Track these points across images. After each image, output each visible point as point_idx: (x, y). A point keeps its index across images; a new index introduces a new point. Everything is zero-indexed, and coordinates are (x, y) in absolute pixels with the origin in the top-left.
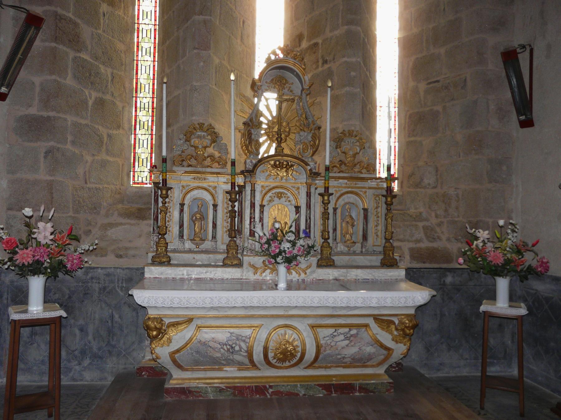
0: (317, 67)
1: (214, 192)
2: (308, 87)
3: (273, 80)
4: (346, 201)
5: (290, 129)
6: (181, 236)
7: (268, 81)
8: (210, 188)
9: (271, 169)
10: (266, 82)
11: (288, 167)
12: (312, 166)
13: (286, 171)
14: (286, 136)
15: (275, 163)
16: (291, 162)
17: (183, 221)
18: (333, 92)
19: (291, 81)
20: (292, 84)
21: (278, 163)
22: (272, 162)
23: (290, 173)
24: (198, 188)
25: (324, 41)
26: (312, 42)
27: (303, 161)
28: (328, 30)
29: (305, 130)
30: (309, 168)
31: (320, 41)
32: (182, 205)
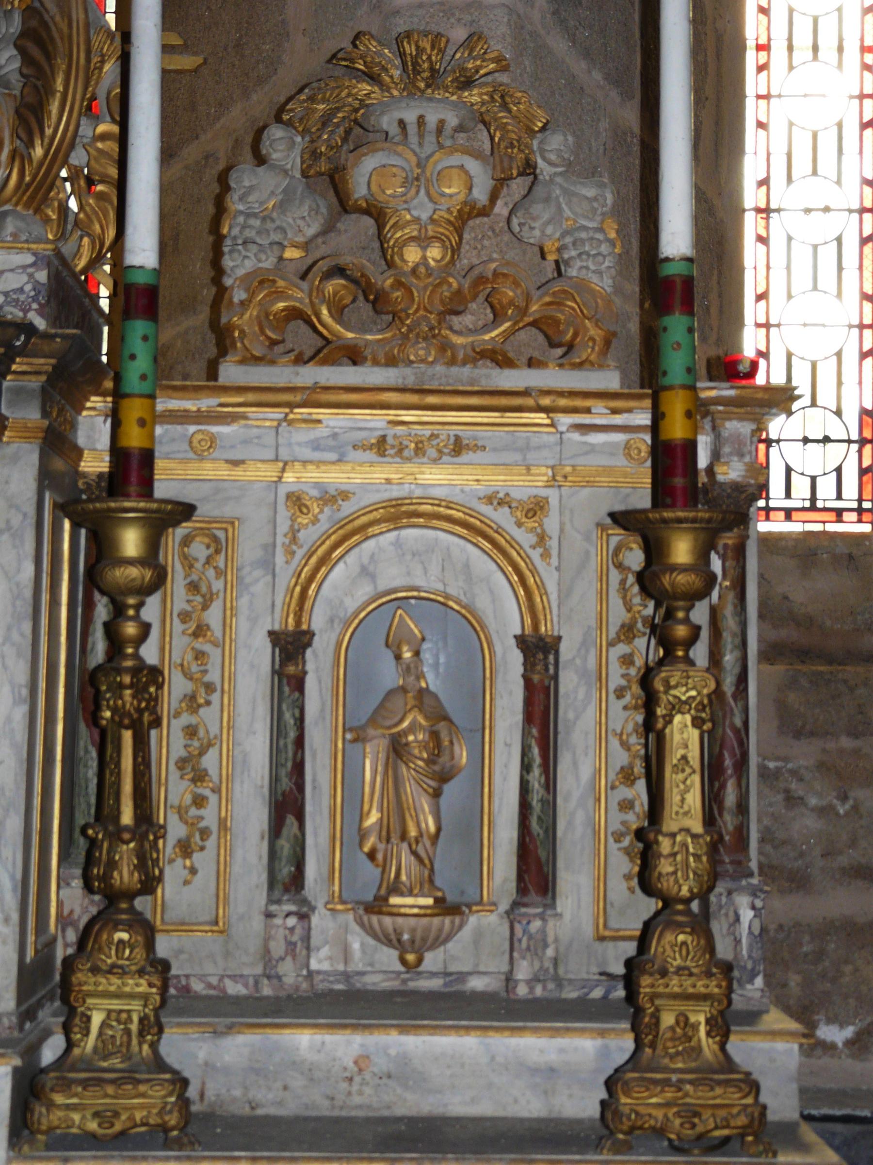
1: (525, 538)
4: (392, 576)
6: (287, 879)
8: (502, 517)
17: (299, 768)
24: (399, 513)
32: (291, 646)
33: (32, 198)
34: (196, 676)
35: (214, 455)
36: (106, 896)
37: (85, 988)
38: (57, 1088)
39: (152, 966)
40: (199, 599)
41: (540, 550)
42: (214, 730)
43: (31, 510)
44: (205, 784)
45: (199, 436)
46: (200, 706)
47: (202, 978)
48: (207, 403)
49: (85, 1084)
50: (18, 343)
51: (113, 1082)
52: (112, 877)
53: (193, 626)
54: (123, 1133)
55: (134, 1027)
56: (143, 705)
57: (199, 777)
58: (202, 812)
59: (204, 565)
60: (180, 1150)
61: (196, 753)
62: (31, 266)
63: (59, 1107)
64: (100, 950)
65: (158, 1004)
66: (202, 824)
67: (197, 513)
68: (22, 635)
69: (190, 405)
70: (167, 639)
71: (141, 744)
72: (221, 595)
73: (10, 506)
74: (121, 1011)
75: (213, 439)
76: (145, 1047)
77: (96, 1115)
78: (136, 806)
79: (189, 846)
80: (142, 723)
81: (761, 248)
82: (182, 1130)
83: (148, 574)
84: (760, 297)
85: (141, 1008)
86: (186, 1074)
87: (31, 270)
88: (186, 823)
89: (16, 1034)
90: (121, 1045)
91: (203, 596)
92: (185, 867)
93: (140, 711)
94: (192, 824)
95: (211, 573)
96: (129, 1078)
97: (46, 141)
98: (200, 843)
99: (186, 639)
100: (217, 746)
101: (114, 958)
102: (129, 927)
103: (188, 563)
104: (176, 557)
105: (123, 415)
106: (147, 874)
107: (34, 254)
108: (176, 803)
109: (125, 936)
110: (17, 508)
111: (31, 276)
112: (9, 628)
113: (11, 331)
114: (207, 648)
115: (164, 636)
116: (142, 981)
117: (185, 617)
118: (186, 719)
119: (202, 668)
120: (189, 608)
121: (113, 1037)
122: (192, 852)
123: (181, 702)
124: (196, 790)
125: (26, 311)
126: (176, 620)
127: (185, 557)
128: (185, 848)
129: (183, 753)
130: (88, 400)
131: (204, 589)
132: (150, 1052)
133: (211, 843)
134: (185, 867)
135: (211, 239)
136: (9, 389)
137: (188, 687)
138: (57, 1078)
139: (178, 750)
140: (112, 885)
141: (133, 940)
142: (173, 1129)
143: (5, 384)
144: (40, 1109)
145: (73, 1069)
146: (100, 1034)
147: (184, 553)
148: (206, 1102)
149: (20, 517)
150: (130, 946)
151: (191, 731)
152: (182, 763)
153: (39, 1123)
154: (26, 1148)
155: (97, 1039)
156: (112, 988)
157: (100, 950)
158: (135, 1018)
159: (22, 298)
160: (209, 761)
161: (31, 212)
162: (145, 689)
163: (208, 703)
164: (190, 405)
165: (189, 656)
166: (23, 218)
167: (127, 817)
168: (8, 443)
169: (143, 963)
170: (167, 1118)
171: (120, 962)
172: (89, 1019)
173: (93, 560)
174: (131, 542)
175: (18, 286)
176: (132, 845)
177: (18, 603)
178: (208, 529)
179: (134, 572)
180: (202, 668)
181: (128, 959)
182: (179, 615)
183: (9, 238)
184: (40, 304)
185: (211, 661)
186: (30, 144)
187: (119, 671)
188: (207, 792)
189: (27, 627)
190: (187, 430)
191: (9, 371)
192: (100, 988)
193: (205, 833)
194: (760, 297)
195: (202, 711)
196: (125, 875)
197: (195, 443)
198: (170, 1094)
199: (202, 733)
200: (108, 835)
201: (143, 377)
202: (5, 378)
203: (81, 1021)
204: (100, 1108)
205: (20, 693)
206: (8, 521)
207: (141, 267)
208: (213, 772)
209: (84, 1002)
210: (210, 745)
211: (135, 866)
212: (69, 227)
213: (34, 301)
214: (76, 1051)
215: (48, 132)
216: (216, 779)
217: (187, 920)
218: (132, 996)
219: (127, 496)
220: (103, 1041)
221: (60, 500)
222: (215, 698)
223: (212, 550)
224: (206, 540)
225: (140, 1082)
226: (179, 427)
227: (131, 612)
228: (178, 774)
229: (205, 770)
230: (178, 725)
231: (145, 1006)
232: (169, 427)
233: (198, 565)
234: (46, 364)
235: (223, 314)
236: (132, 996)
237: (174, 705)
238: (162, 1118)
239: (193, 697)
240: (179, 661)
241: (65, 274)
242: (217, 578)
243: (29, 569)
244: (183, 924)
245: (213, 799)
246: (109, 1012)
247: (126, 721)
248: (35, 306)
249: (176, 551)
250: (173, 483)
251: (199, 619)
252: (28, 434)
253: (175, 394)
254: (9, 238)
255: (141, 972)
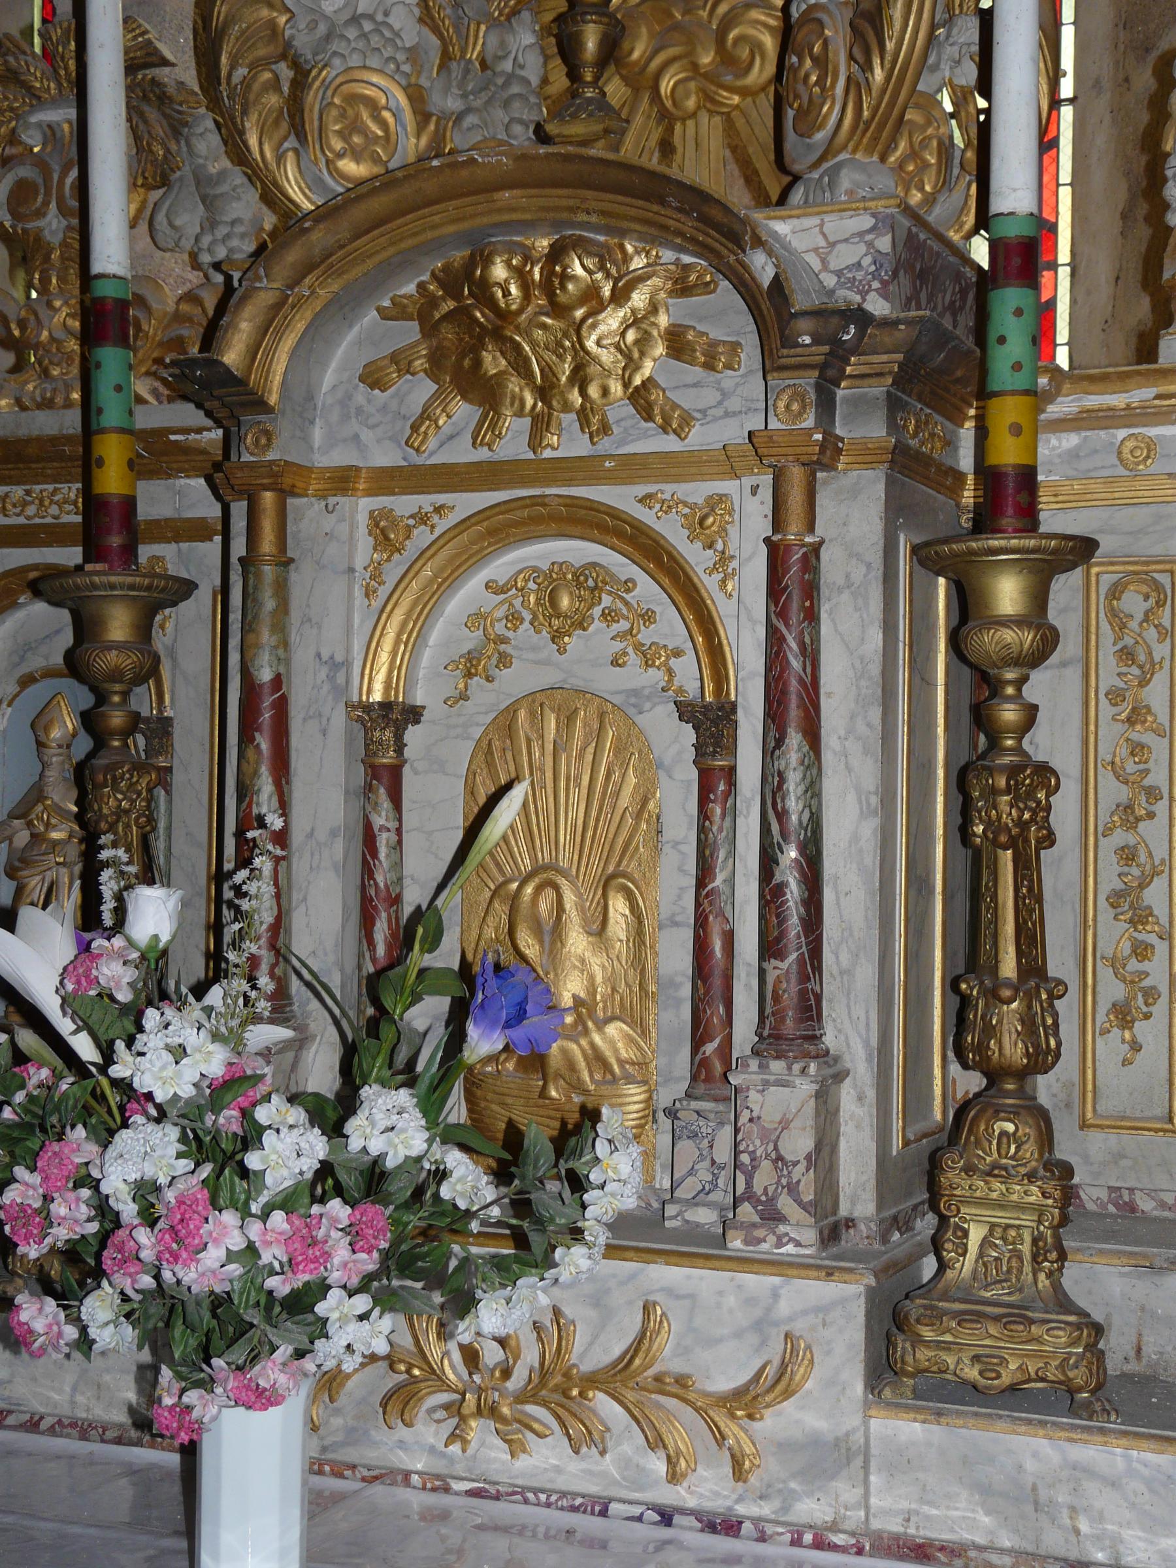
33: (875, 139)
34: (1132, 778)
35: (1152, 470)
36: (985, 1074)
37: (958, 1192)
38: (926, 1321)
39: (1045, 1168)
40: (1135, 671)
41: (435, 519)
42: (1160, 853)
43: (876, 557)
44: (1148, 928)
45: (1130, 444)
46: (1138, 820)
47: (1151, 1193)
48: (1141, 395)
49: (962, 1318)
50: (846, 337)
51: (996, 1319)
52: (988, 1047)
53: (1125, 711)
54: (1013, 1388)
55: (1026, 1248)
56: (1027, 816)
57: (1140, 917)
58: (1145, 966)
59: (1141, 624)
60: (1090, 1419)
61: (1135, 884)
63: (928, 1344)
64: (978, 1143)
65: (1056, 1222)
66: (1147, 983)
67: (1097, 553)
68: (869, 725)
69: (1117, 400)
70: (1092, 728)
71: (1027, 869)
72: (1167, 664)
73: (851, 556)
74: (1008, 1226)
75: (1151, 446)
76: (1042, 1276)
77: (976, 1358)
78: (1019, 953)
79: (1130, 1012)
80: (1027, 841)
82: (1093, 1392)
83: (1028, 638)
85: (1034, 1224)
86: (1098, 1316)
87: (869, 237)
88: (1124, 981)
89: (877, 1246)
90: (1009, 1271)
91: (1141, 667)
92: (1123, 1041)
93: (1023, 825)
94: (1132, 982)
95: (1151, 634)
96: (1016, 1317)
97: (888, 58)
98: (1145, 1009)
99: (1119, 727)
100: (1166, 875)
101: (995, 1155)
102: (1013, 1114)
103: (1119, 620)
104: (1102, 615)
105: (990, 423)
106: (1037, 1046)
107: (874, 215)
108: (1109, 953)
109: (1010, 1127)
110: (858, 556)
111: (870, 244)
112: (852, 717)
113: (835, 321)
114: (1148, 738)
115: (1087, 724)
116: (1034, 1189)
117: (1116, 696)
118: (1120, 837)
119: (1142, 766)
120: (1122, 685)
121: (996, 1259)
122: (1133, 1021)
123: (1112, 814)
124: (1136, 934)
125: (864, 294)
126: (1103, 700)
127: (1113, 613)
128: (1123, 1015)
129: (1118, 885)
130: (1044, 411)
131: (1142, 658)
132: (1047, 1282)
133: (1160, 1008)
134: (1123, 1041)
135: (1144, 159)
136: (845, 400)
137: (1123, 793)
138: (925, 1307)
139: (1110, 881)
140: (989, 1058)
141: (1020, 1133)
142: (1080, 1390)
143: (840, 393)
144: (902, 1343)
145: (945, 1297)
146: (981, 1255)
147: (1113, 609)
148: (1144, 1361)
149: (863, 569)
150: (1015, 1142)
151: (1128, 855)
152: (1116, 899)
153: (903, 1362)
154: (887, 1393)
155: (977, 1261)
156: (994, 1195)
157: (978, 1143)
158: (1027, 1238)
159: (859, 275)
160: (1154, 895)
161: (875, 158)
162: (1031, 794)
163: (1151, 815)
164: (1117, 400)
165: (1124, 751)
166: (862, 168)
167: (1009, 967)
168: (845, 471)
169: (1034, 1163)
170: (1071, 1374)
171: (1004, 1161)
172: (966, 1233)
173: (955, 622)
174: (1007, 593)
175: (855, 260)
176: (1014, 1005)
177: (863, 683)
178: (1146, 573)
179: (1008, 635)
180: (1142, 766)
181: (1012, 1158)
182: (1106, 695)
183: (843, 198)
184: (883, 282)
185: (1154, 756)
186: (867, 67)
187: (991, 771)
188: (1153, 939)
189: (875, 714)
190: (1115, 436)
191: (842, 375)
192: (978, 1194)
193: (1151, 995)
195: (1141, 825)
196: (1011, 1048)
197: (1126, 454)
198: (1073, 1344)
199: (1143, 857)
200: (984, 992)
201: (1017, 367)
202: (839, 386)
203: (954, 1233)
204: (981, 1351)
205: (868, 804)
206: (848, 576)
207: (1012, 214)
208: (1160, 911)
209: (959, 1211)
210: (1155, 873)
211: (1019, 1034)
212: (956, 171)
214: (950, 1274)
215: (890, 46)
216: (1164, 920)
217: (1128, 1114)
218: (1021, 1207)
219: (997, 530)
220: (985, 1264)
221: (917, 540)
222: (1161, 807)
223: (1152, 601)
224: (1145, 589)
225: (1032, 1322)
226: (1102, 433)
227: (1010, 690)
228: (1112, 912)
229: (1150, 907)
230: (1109, 845)
231: (1040, 1222)
232: (1088, 433)
233: (1134, 624)
234: (891, 361)
235: (1166, 267)
236: (1021, 1207)
237: (1104, 817)
238: (1064, 1373)
239: (1129, 808)
240: (1109, 758)
241: (922, 236)
242: (1160, 641)
243: (876, 637)
244: (1123, 1118)
245: (1161, 947)
246: (993, 1226)
247: (1003, 838)
248: (876, 285)
249: (1101, 607)
250: (1095, 511)
251: (1135, 700)
252: (869, 458)
253: (1092, 388)
255: (1031, 1177)
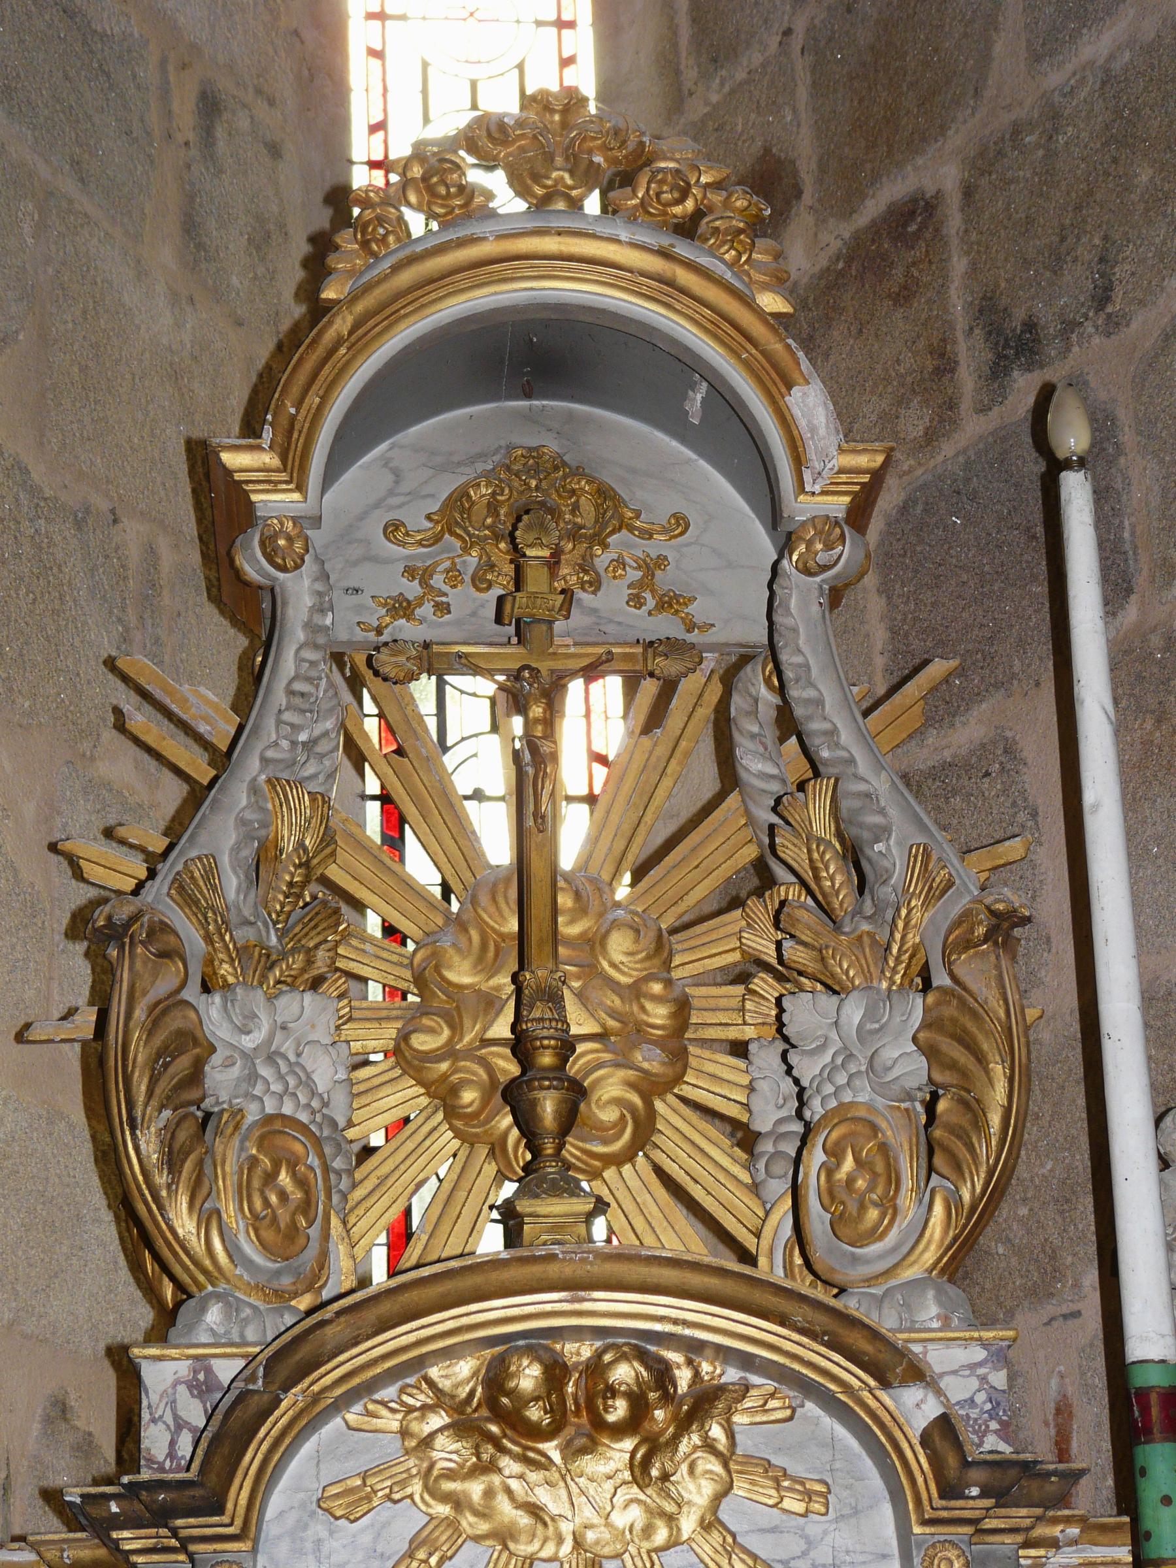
0: (946, 415)
2: (838, 505)
3: (459, 502)
5: (682, 1007)
7: (416, 519)
9: (449, 1451)
10: (393, 529)
11: (662, 1412)
12: (958, 1389)
13: (640, 1471)
14: (651, 1088)
15: (496, 1380)
16: (694, 1348)
18: (1131, 614)
19: (654, 502)
20: (680, 523)
21: (528, 1376)
22: (461, 1374)
23: (696, 1491)
25: (984, 162)
26: (873, 208)
27: (841, 1331)
28: (1007, 48)
29: (845, 967)
30: (917, 1409)
31: (939, 172)
62: (980, 1364)
81: (375, 63)
84: (374, 128)
111: (983, 1379)
175: (967, 1396)
183: (936, 1324)
184: (1001, 1422)
194: (374, 128)
213: (991, 1418)
254: (936, 1324)
